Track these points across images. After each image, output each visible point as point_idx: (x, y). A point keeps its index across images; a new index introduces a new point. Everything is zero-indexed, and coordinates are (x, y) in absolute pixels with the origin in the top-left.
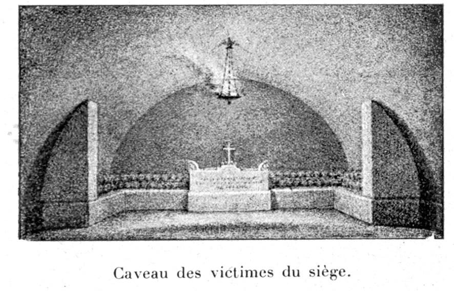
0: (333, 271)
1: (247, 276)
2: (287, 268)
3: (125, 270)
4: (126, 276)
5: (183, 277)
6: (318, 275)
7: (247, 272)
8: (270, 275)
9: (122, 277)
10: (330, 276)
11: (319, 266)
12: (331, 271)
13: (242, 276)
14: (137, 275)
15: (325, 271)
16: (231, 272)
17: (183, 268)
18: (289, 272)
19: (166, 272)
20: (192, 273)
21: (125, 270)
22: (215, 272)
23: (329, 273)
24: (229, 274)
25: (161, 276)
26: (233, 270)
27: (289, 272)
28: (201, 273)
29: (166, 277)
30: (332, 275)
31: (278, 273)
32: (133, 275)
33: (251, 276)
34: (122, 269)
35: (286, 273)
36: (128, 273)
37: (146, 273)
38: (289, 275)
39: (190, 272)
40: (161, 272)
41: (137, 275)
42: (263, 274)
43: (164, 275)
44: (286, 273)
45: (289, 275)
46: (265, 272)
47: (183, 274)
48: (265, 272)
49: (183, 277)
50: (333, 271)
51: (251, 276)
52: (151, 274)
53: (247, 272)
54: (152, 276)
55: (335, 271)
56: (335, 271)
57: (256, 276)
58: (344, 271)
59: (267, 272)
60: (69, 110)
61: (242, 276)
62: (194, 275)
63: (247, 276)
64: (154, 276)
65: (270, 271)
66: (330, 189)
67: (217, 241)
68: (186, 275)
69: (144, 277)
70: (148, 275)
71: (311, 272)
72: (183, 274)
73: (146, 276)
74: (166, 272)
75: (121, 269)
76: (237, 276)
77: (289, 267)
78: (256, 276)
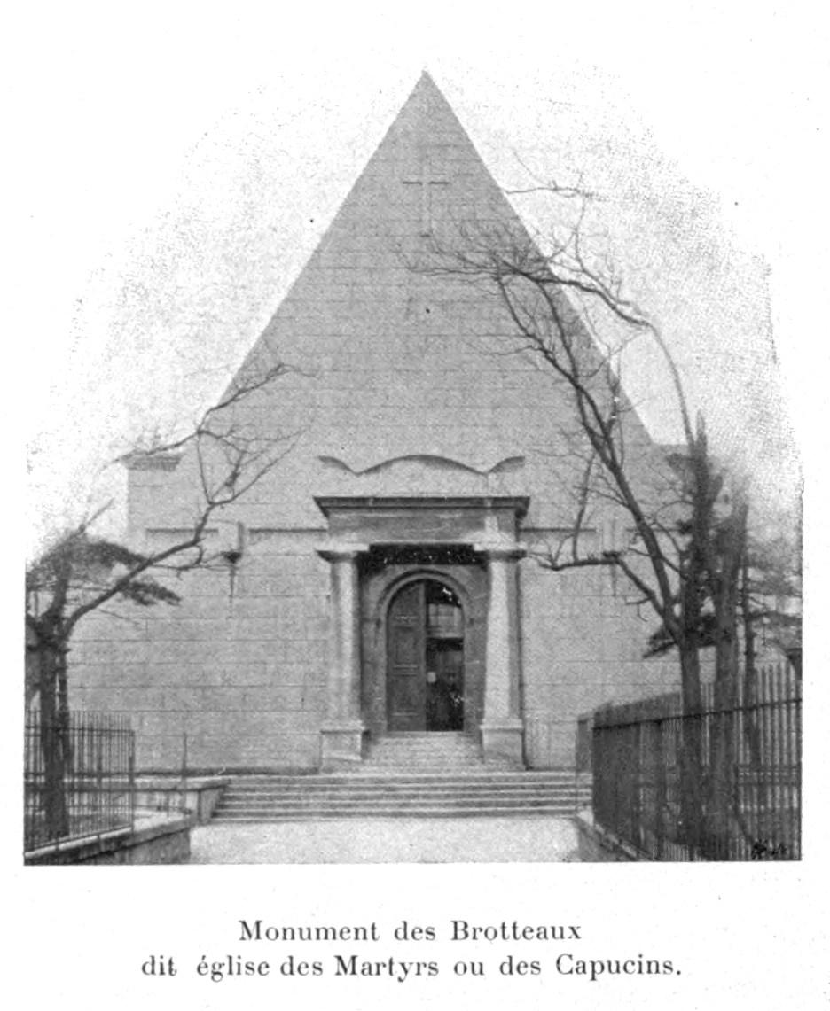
0: (217, 966)
1: (318, 938)
3: (576, 959)
4: (577, 970)
5: (291, 973)
7: (649, 963)
9: (571, 972)
10: (210, 975)
12: (213, 966)
13: (640, 972)
14: (404, 968)
15: (203, 965)
16: (633, 963)
19: (481, 965)
20: (526, 966)
21: (576, 959)
22: (407, 966)
23: (210, 968)
24: (629, 967)
26: (387, 963)
28: (322, 967)
30: (215, 973)
32: (568, 932)
33: (326, 938)
34: (570, 956)
41: (404, 968)
42: (304, 970)
43: (477, 969)
45: (153, 972)
49: (291, 973)
50: (217, 966)
51: (326, 938)
52: (536, 932)
53: (649, 963)
54: (538, 935)
55: (220, 966)
56: (220, 966)
57: (334, 938)
58: (267, 966)
59: (529, 965)
61: (640, 972)
62: (530, 969)
63: (318, 938)
64: (542, 936)
68: (295, 969)
71: (319, 969)
73: (529, 935)
74: (481, 965)
75: (568, 959)
76: (518, 936)
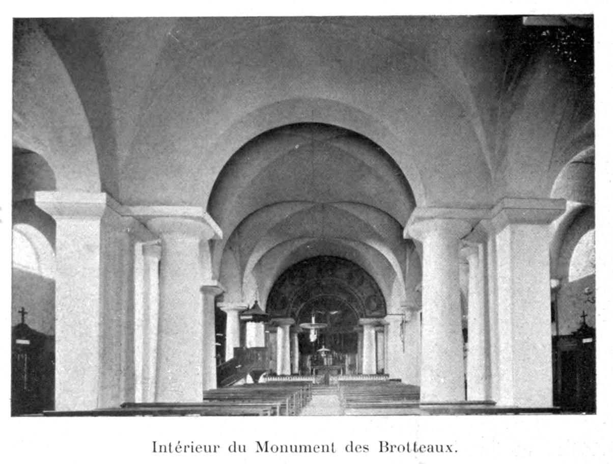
1: (301, 451)
2: (350, 444)
6: (266, 451)
8: (366, 450)
11: (179, 442)
15: (179, 447)
17: (352, 442)
18: (235, 448)
25: (291, 450)
27: (235, 448)
29: (244, 451)
31: (340, 447)
32: (445, 448)
35: (232, 449)
36: (430, 447)
37: (199, 447)
38: (235, 451)
39: (317, 447)
40: (437, 446)
44: (232, 449)
46: (361, 447)
47: (351, 448)
48: (361, 447)
51: (305, 451)
52: (427, 448)
57: (310, 451)
60: (308, 136)
62: (362, 449)
65: (366, 447)
66: (339, 240)
67: (242, 417)
68: (269, 449)
69: (421, 451)
70: (424, 449)
72: (351, 448)
73: (179, 450)
77: (235, 442)
78: (310, 451)
